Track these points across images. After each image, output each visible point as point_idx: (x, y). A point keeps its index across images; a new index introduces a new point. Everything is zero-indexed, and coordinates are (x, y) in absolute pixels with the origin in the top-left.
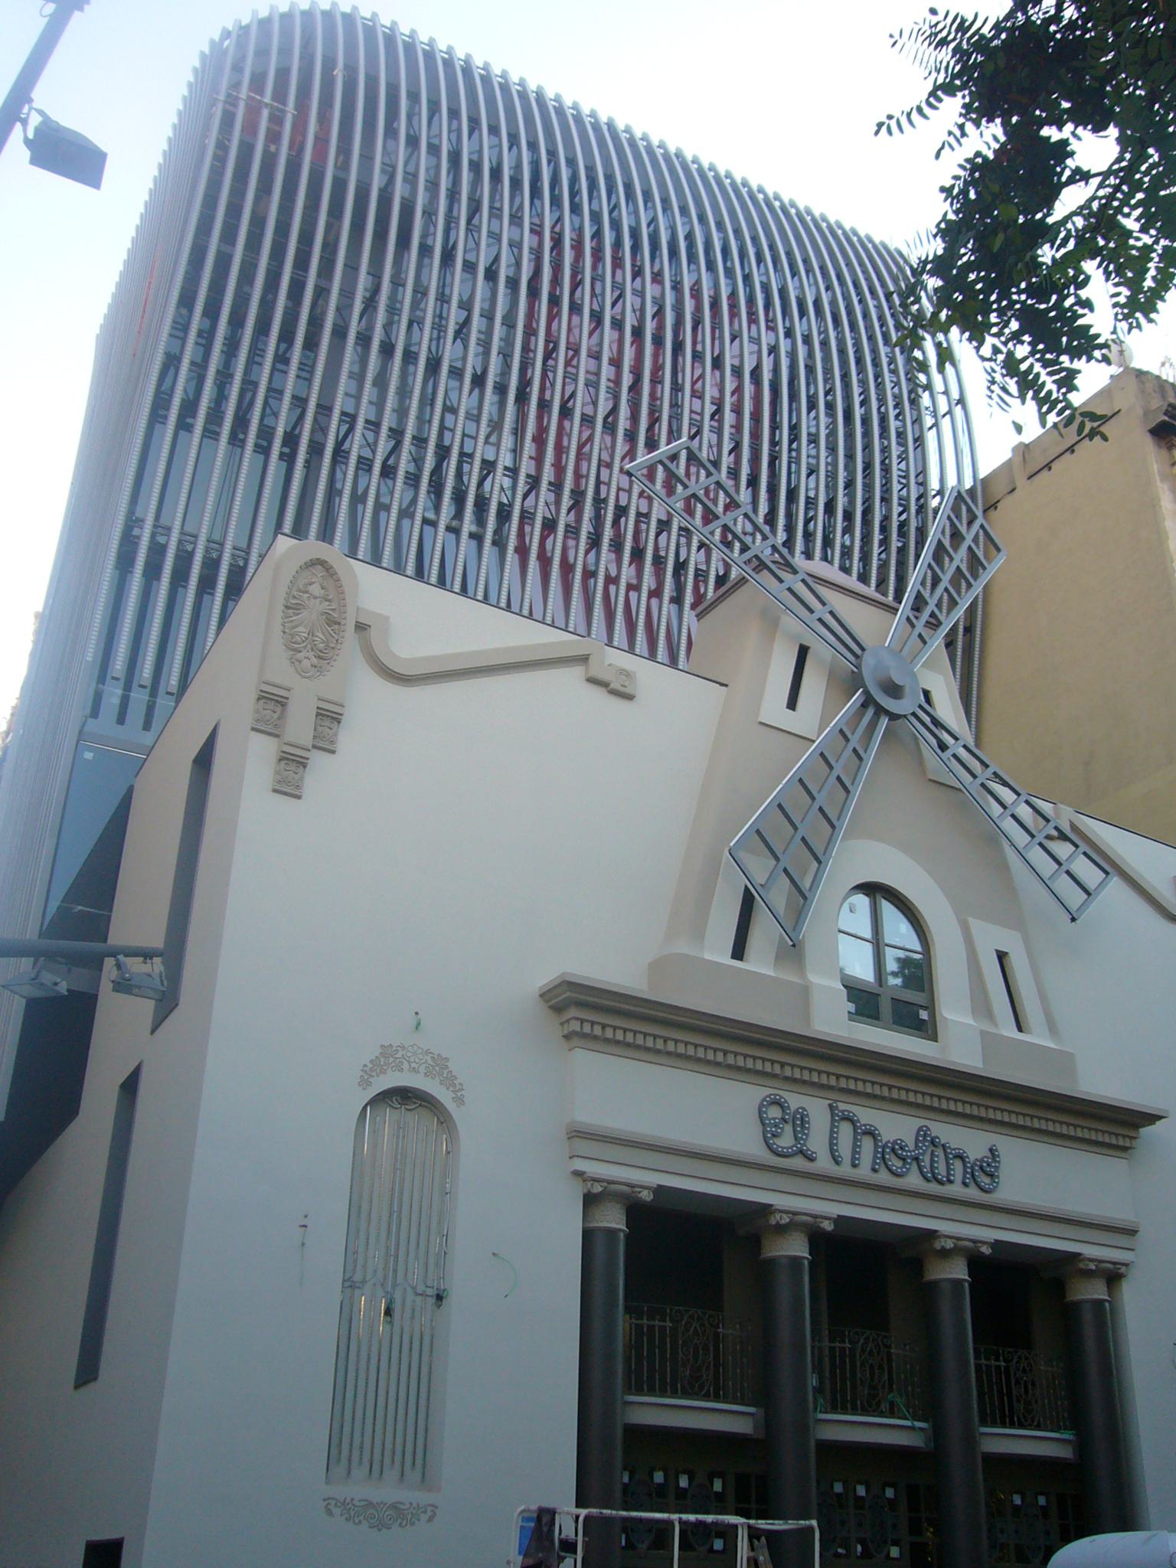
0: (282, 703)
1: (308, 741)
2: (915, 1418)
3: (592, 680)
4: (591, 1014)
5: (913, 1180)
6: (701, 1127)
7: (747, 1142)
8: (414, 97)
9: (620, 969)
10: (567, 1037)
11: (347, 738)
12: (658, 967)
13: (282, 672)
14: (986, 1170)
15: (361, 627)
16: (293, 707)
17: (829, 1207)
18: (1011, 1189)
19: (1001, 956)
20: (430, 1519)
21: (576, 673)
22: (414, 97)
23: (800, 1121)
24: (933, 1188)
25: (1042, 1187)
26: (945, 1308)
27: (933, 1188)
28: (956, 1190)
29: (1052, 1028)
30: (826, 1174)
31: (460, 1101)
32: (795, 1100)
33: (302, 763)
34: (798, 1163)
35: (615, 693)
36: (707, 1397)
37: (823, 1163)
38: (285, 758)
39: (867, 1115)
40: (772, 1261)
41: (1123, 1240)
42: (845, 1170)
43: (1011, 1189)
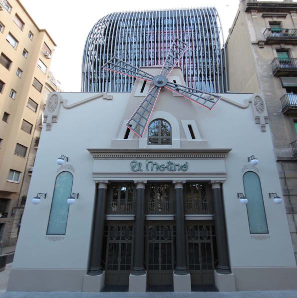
0: (259, 119)
1: (265, 123)
2: (209, 214)
3: (104, 99)
4: (97, 153)
5: (166, 171)
6: (120, 169)
7: (129, 170)
8: (206, 16)
9: (104, 144)
10: (94, 157)
11: (59, 121)
12: (113, 142)
13: (257, 114)
14: (186, 166)
15: (62, 102)
16: (261, 119)
17: (145, 179)
18: (190, 170)
19: (190, 127)
20: (269, 238)
21: (102, 98)
22: (206, 16)
23: (140, 164)
24: (171, 172)
25: (199, 169)
26: (139, 194)
27: (171, 172)
28: (177, 172)
29: (202, 136)
30: (145, 172)
31: (258, 172)
32: (138, 161)
33: (265, 127)
34: (139, 172)
35: (108, 100)
36: (123, 214)
37: (145, 171)
38: (47, 126)
39: (154, 161)
40: (213, 189)
41: (224, 176)
42: (150, 172)
43: (190, 170)
